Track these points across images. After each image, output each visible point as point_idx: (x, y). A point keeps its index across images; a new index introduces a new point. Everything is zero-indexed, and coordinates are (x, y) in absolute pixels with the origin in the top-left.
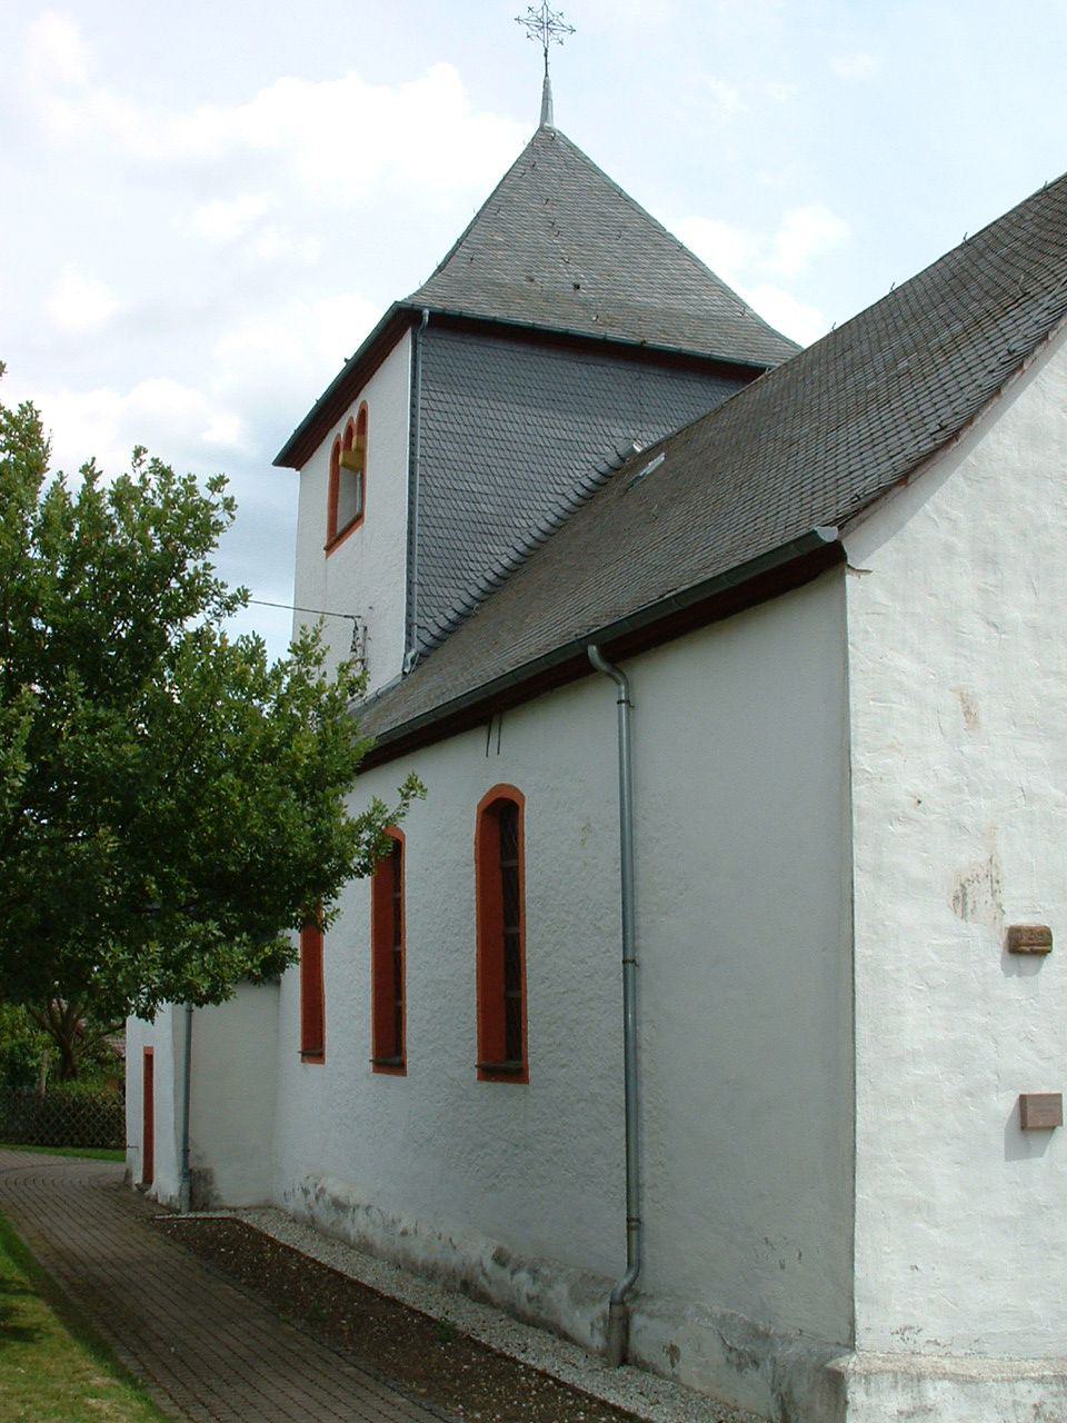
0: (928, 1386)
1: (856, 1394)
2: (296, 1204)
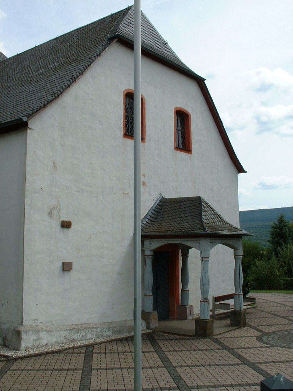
0: (40, 333)
1: (24, 336)
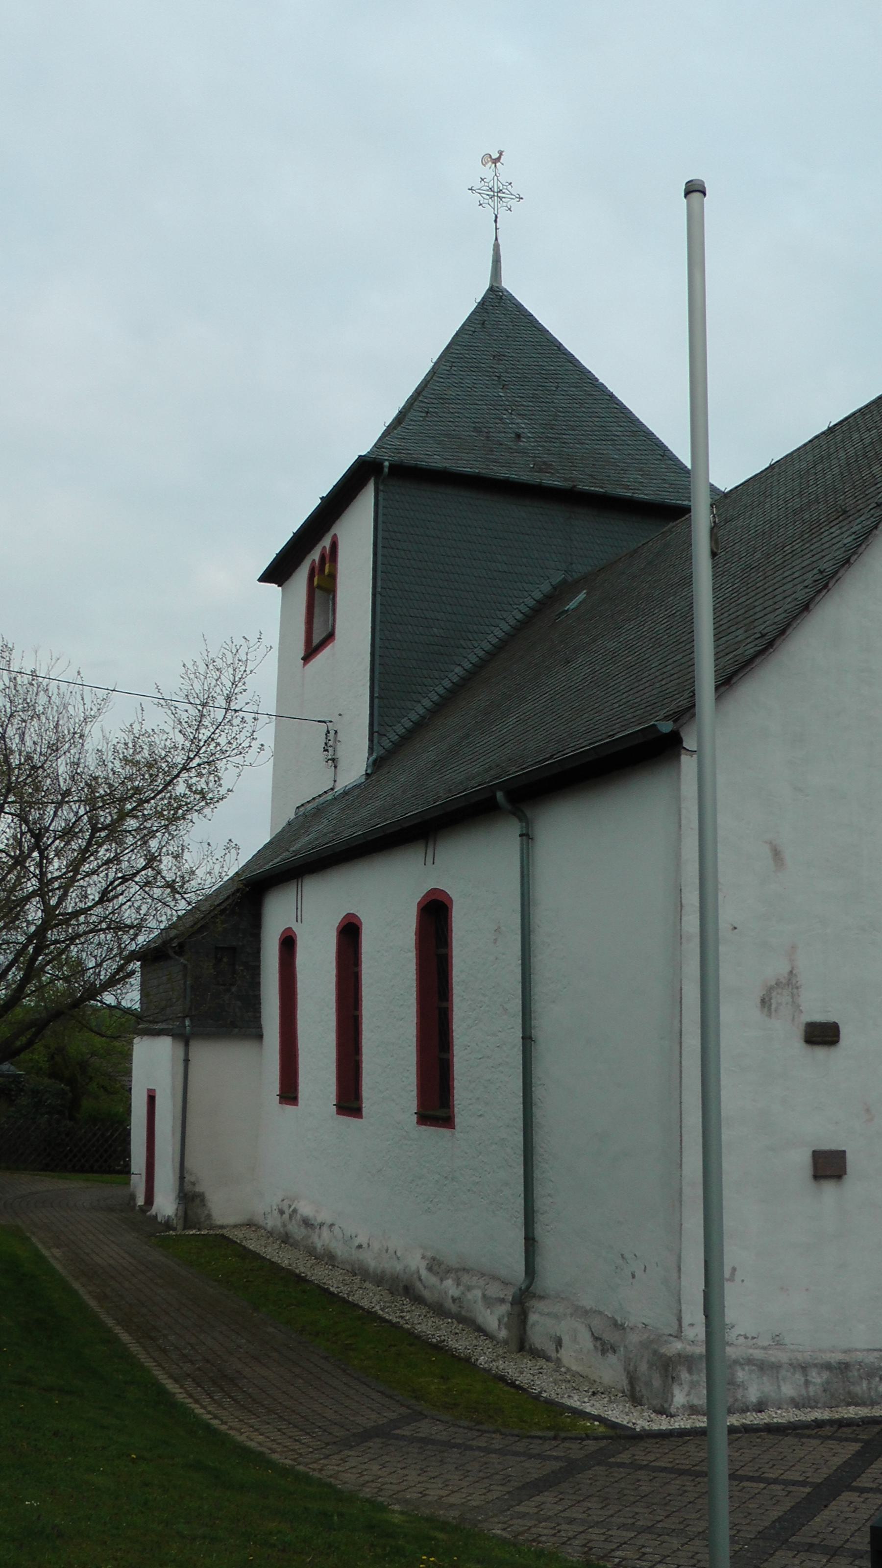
2: (272, 1222)
